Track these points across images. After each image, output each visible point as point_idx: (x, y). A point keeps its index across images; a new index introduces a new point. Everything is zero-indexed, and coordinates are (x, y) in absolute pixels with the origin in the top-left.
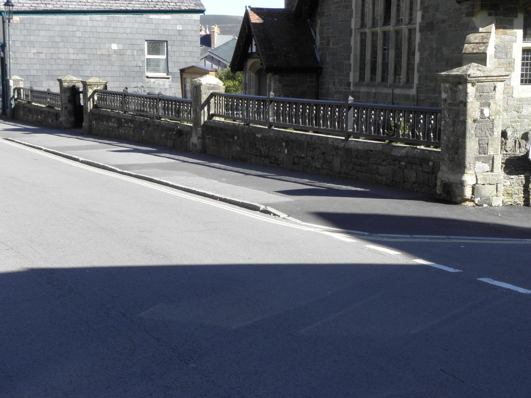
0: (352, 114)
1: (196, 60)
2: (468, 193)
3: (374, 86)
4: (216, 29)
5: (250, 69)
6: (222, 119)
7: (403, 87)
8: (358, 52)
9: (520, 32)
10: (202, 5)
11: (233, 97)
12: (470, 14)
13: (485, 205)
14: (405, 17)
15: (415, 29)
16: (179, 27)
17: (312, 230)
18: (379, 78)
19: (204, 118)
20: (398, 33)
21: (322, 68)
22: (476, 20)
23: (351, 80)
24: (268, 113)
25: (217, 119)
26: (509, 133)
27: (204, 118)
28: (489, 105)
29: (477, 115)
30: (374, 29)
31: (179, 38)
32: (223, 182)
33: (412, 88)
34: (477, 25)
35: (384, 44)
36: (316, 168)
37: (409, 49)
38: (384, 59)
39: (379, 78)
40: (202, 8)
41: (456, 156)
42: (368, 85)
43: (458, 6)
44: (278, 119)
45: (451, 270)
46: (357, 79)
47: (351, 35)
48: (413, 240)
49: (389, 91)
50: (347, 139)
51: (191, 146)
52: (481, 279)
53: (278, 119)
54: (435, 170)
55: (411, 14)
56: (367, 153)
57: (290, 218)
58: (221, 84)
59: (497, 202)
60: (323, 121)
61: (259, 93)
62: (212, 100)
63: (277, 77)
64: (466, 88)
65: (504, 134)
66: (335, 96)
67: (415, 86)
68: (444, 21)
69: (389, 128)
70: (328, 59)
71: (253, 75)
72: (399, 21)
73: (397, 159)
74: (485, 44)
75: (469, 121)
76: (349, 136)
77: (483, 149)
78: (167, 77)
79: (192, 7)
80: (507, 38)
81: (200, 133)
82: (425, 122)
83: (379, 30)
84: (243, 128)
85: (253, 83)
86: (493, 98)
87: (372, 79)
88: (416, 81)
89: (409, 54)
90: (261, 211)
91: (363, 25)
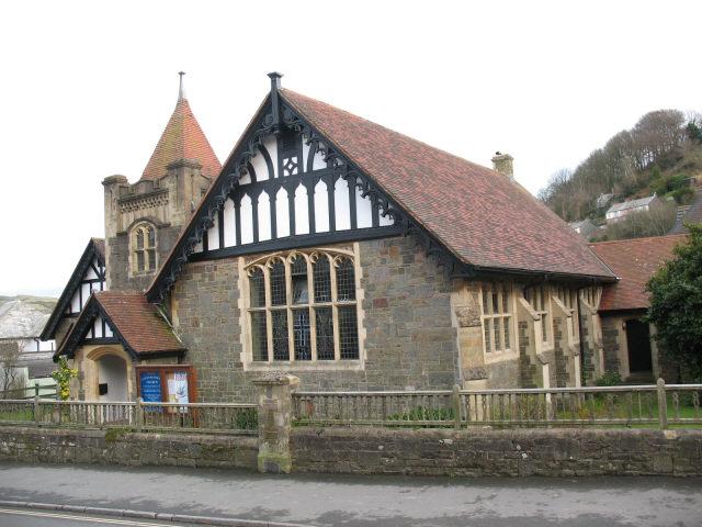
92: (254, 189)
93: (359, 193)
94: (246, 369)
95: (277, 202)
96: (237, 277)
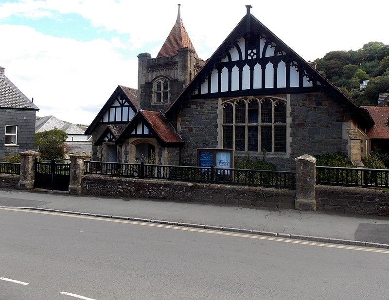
92: (230, 65)
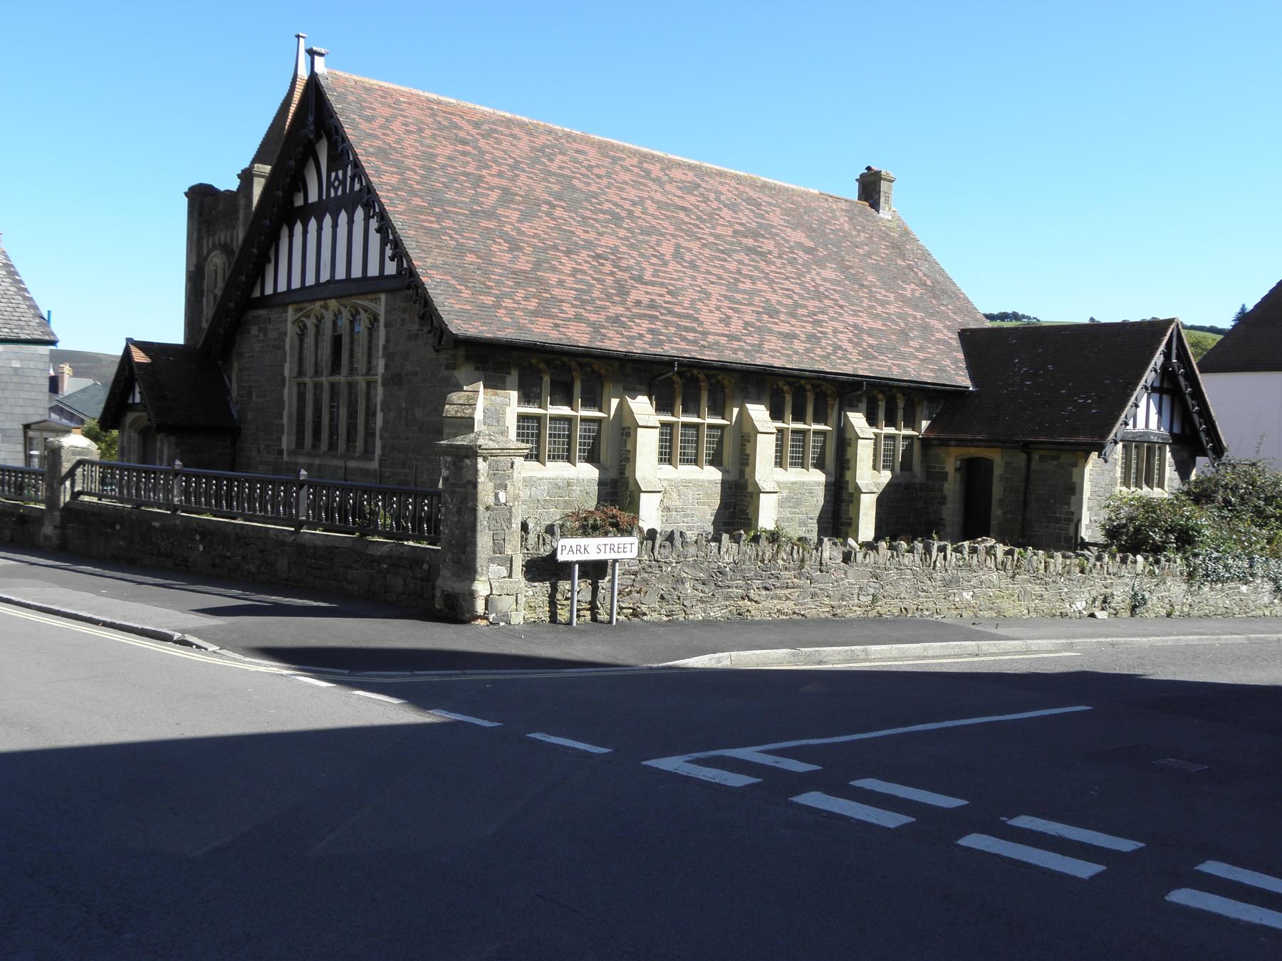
0: (306, 495)
1: (41, 411)
2: (480, 607)
3: (317, 456)
4: (67, 369)
5: (131, 425)
6: (95, 500)
7: (359, 459)
8: (294, 409)
9: (514, 395)
10: (52, 334)
11: (111, 467)
12: (452, 367)
13: (502, 624)
14: (361, 365)
15: (376, 382)
16: (16, 364)
17: (262, 669)
18: (324, 445)
19: (65, 497)
20: (351, 385)
21: (240, 429)
22: (460, 374)
23: (284, 446)
24: (171, 491)
25: (86, 498)
26: (531, 526)
27: (65, 497)
28: (505, 487)
29: (490, 500)
30: (300, 380)
31: (16, 379)
32: (102, 595)
33: (373, 459)
34: (461, 382)
35: (332, 400)
36: (249, 572)
37: (368, 407)
38: (331, 419)
39: (324, 445)
40: (52, 338)
41: (463, 556)
42: (309, 454)
43: (434, 355)
44: (188, 500)
45: (487, 724)
46: (293, 446)
47: (283, 385)
48: (416, 679)
49: (340, 463)
50: (297, 531)
51: (42, 539)
52: (532, 735)
53: (188, 500)
54: (430, 577)
55: (369, 362)
56: (329, 552)
57: (224, 652)
58: (93, 446)
59: (517, 619)
60: (249, 503)
61: (143, 460)
62: (79, 471)
63: (173, 438)
64: (476, 463)
65: (524, 527)
66: (260, 467)
67: (377, 458)
68: (415, 374)
69: (362, 515)
70: (250, 416)
71: (134, 435)
72: (352, 371)
73: (374, 560)
74: (473, 406)
75: (481, 508)
76: (176, 510)
77: (498, 547)
78: (45, 434)
79: (37, 335)
80: (499, 399)
81: (59, 519)
82: (415, 508)
83: (325, 380)
84: (130, 512)
85: (135, 446)
86: (510, 477)
87: (316, 445)
88: (378, 451)
89: (367, 415)
90: (176, 642)
91: (301, 373)
93: (1219, 337)
94: (285, 458)
95: (339, 229)
96: (285, 334)
